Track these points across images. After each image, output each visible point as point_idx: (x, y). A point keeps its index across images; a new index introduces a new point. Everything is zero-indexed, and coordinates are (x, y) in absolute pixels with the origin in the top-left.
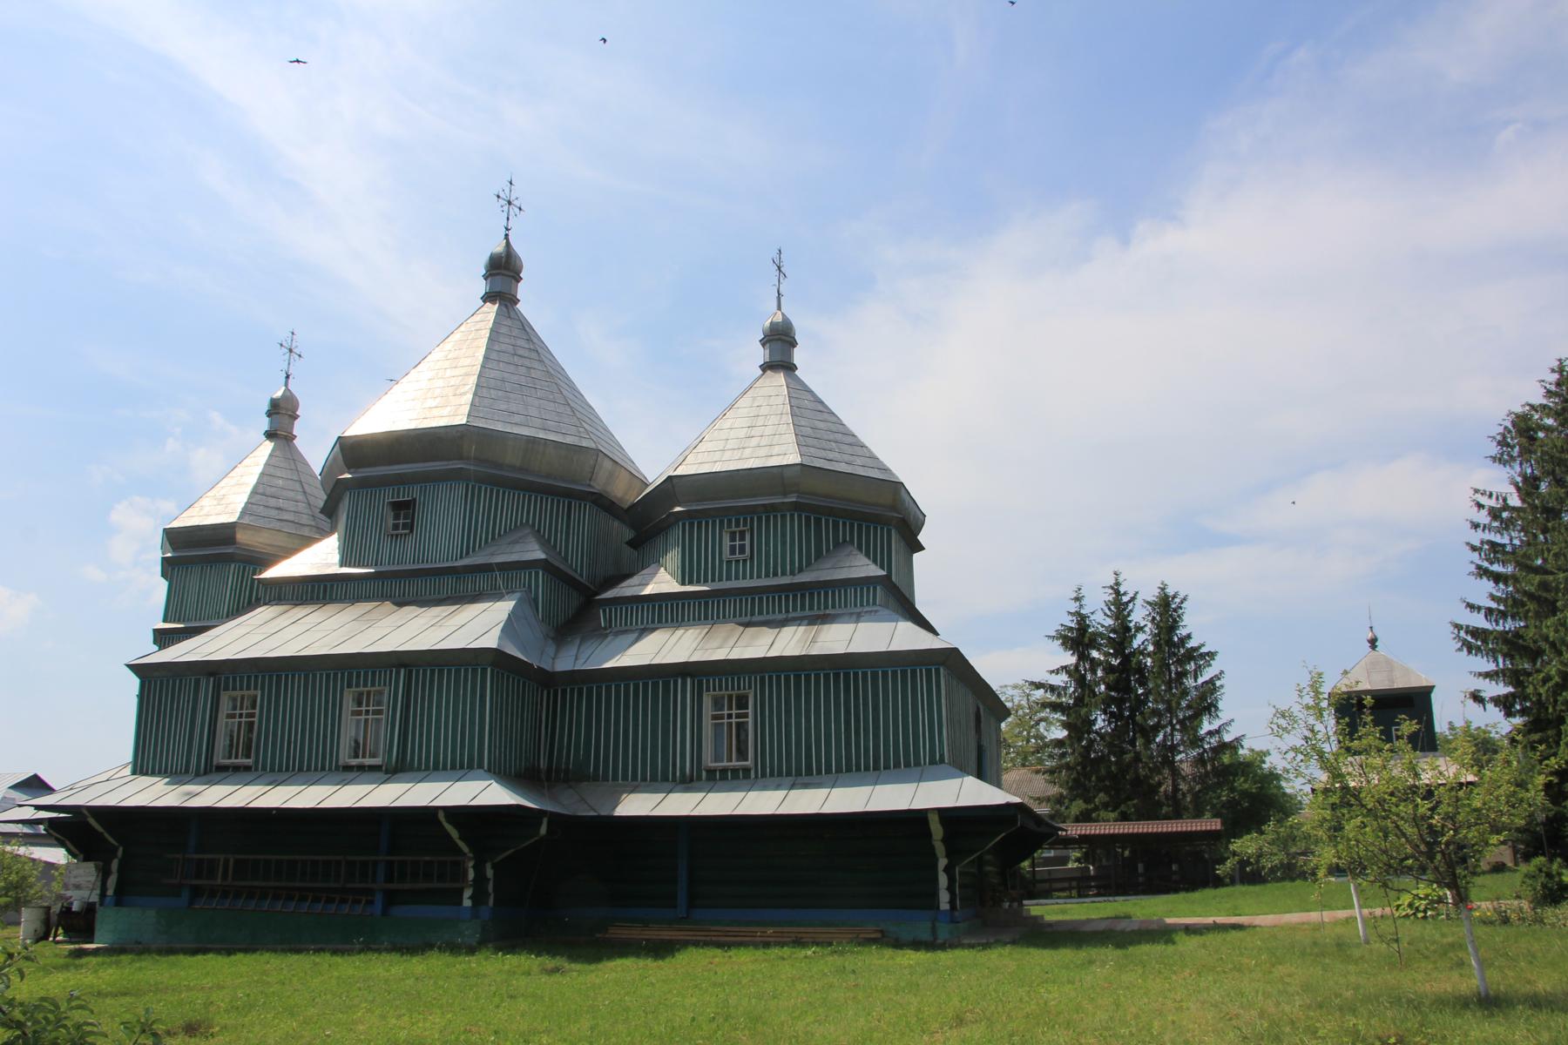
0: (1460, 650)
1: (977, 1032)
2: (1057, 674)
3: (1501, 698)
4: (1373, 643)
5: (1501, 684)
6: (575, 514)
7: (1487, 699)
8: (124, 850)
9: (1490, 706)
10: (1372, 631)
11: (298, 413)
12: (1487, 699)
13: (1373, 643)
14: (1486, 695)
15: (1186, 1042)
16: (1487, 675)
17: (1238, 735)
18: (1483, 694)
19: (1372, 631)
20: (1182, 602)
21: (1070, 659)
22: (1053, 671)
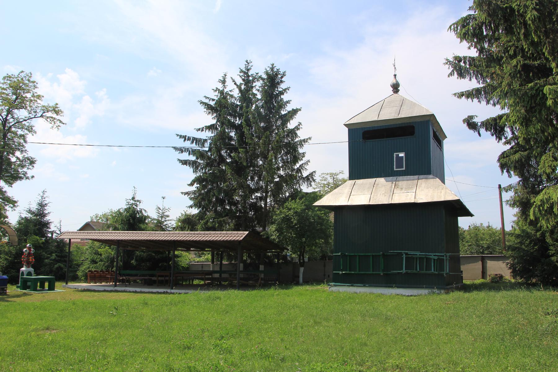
0: (451, 74)
1: (374, 369)
2: (202, 130)
3: (490, 121)
4: (396, 88)
5: (474, 80)
6: (446, 263)
7: (479, 124)
8: (6, 279)
9: (482, 131)
10: (395, 78)
11: (461, 270)
12: (479, 124)
13: (396, 88)
14: (478, 120)
15: (464, 371)
16: (470, 95)
17: (312, 171)
18: (475, 120)
19: (395, 78)
20: (282, 77)
21: (211, 120)
22: (199, 130)
